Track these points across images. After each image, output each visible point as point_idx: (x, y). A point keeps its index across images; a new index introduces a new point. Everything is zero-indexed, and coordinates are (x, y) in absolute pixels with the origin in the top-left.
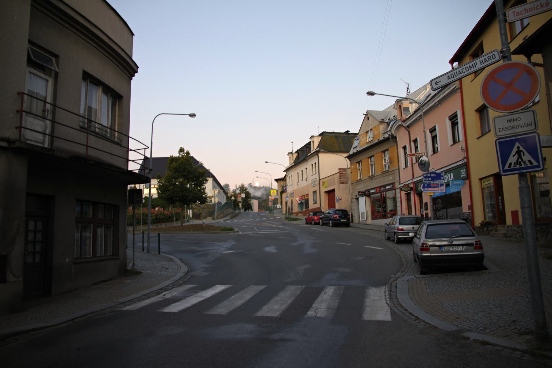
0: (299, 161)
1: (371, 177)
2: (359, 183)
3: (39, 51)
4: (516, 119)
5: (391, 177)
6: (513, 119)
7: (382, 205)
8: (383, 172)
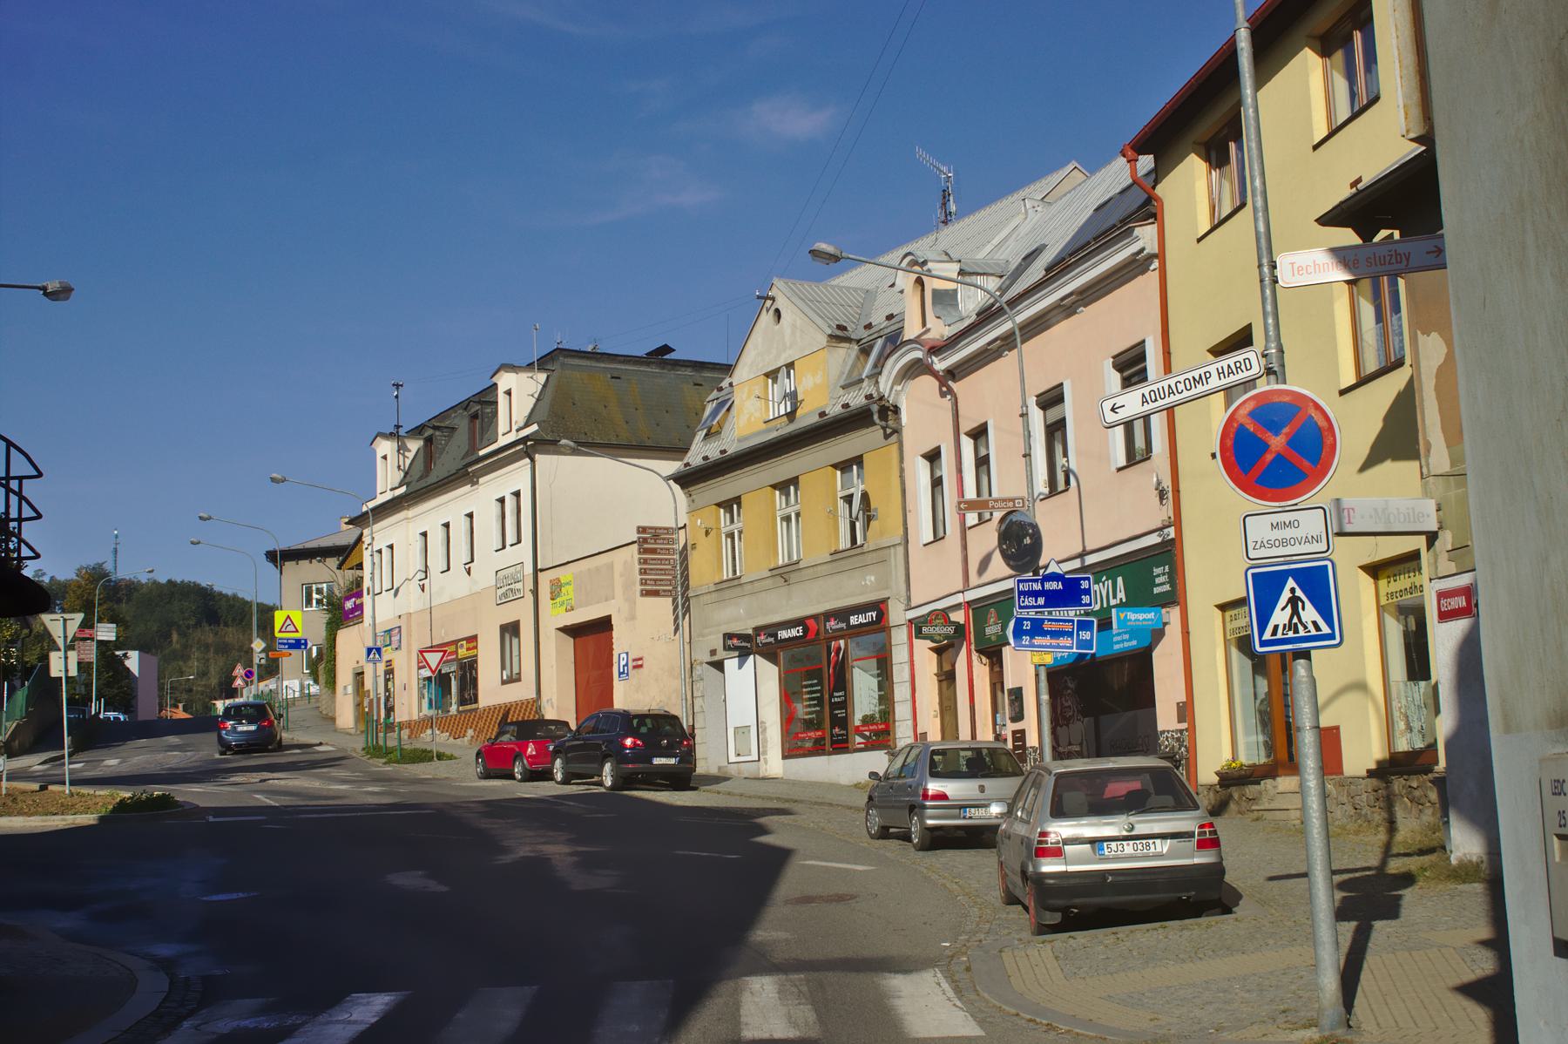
0: (432, 479)
1: (781, 571)
2: (727, 594)
3: (496, 458)
4: (1290, 522)
5: (873, 578)
6: (1285, 523)
7: (831, 696)
8: (836, 552)
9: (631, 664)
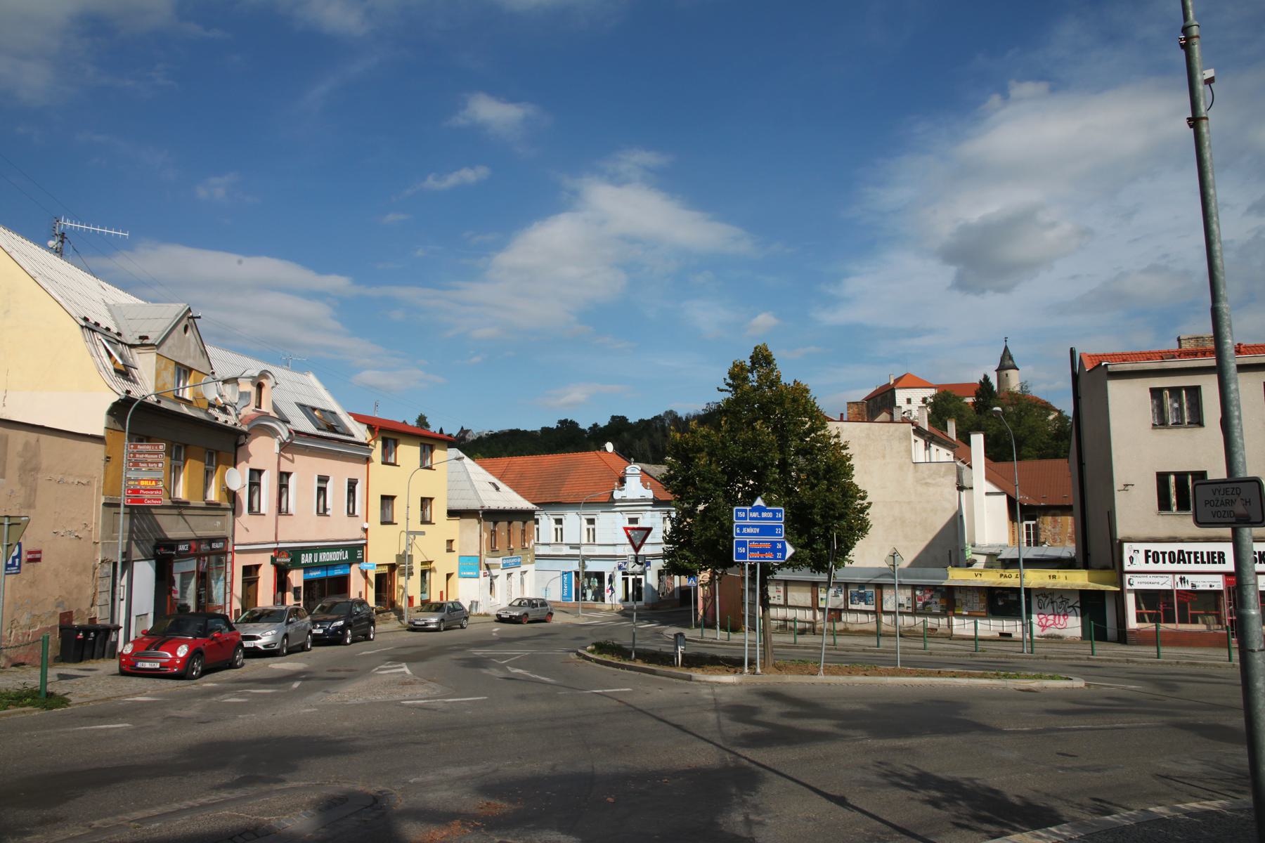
9: (24, 556)
